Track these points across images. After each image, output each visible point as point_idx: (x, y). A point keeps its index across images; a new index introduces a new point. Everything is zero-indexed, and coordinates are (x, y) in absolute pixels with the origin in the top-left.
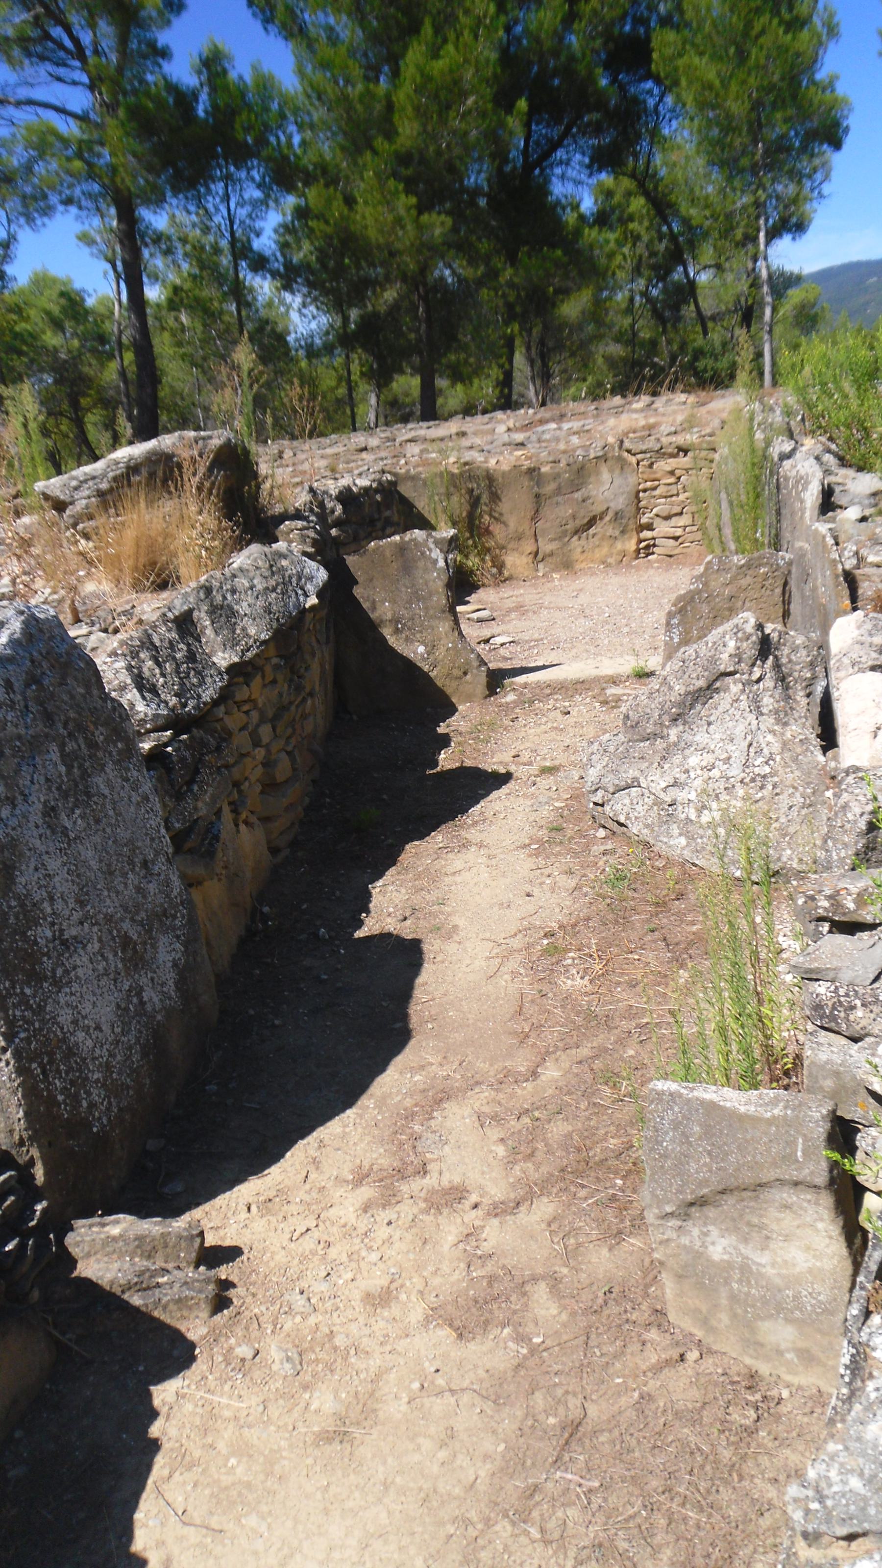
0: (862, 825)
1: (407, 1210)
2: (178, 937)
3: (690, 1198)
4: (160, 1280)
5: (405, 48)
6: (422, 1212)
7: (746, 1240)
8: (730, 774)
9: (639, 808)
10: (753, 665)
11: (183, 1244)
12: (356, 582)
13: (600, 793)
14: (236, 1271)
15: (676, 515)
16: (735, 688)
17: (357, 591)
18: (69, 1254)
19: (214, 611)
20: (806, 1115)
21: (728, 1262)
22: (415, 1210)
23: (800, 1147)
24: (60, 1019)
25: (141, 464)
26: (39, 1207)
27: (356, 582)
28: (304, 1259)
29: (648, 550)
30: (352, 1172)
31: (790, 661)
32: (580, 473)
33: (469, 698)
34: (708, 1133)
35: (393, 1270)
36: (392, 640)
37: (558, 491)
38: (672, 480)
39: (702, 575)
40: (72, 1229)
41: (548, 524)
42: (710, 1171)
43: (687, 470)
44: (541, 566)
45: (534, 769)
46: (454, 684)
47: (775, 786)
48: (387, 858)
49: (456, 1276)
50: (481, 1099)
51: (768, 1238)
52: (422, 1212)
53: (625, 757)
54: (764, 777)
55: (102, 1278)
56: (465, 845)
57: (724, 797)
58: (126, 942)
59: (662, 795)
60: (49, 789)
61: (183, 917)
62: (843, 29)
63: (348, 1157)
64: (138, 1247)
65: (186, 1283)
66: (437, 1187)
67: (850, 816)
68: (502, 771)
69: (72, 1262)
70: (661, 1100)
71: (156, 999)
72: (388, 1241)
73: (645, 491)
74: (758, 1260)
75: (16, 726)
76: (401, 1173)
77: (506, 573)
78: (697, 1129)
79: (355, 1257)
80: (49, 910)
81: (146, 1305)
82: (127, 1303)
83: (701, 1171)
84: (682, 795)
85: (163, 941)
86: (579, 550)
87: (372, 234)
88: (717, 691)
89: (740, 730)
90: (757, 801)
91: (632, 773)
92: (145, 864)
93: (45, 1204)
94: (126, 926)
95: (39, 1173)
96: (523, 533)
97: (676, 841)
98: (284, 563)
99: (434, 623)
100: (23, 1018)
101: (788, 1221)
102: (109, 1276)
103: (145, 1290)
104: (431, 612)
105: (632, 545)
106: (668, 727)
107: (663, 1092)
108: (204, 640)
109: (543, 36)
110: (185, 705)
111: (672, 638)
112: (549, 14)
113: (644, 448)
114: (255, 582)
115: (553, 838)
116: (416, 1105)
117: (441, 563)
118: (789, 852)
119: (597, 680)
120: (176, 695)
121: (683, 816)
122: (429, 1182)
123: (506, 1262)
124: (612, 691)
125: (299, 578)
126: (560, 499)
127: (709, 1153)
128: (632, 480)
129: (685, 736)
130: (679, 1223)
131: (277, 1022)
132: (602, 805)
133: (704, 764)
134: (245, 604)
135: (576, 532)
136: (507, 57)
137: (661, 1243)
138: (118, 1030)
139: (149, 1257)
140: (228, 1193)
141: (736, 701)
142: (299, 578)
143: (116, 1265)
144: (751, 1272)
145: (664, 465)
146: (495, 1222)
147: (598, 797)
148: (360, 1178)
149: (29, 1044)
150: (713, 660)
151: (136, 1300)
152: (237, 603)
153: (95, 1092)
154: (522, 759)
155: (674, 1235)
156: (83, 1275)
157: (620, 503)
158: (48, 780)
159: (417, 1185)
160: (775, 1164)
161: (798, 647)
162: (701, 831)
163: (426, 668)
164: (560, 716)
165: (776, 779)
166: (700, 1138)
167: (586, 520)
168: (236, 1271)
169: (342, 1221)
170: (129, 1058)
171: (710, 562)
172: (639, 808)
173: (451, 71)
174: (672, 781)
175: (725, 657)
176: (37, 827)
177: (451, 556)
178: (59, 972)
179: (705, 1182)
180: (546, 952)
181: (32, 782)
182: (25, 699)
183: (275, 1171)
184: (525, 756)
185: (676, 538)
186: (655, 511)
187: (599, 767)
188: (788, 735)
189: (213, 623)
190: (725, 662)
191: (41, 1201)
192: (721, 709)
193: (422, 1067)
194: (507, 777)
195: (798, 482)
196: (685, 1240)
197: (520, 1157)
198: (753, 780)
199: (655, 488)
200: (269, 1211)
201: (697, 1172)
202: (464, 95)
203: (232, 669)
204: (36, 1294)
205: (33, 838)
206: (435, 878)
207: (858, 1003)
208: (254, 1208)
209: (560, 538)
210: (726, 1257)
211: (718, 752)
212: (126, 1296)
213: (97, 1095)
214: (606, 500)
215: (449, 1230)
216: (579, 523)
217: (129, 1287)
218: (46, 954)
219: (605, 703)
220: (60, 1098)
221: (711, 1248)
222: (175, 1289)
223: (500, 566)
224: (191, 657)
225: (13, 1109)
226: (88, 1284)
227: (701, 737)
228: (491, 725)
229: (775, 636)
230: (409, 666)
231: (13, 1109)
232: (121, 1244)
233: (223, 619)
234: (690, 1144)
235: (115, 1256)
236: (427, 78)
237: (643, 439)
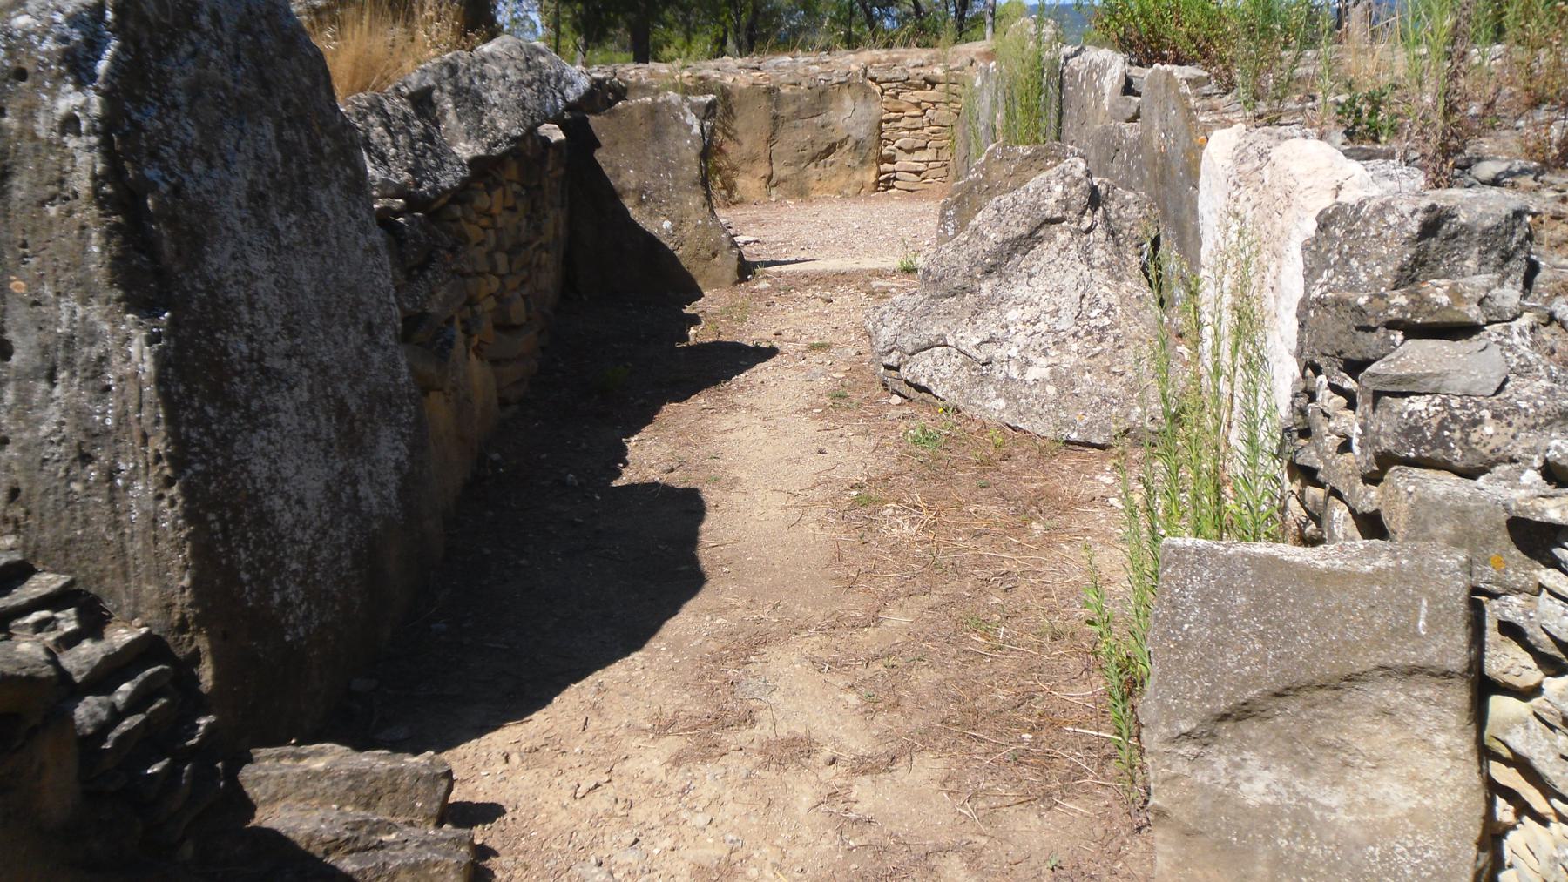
0: (1414, 227)
1: (738, 765)
2: (403, 435)
3: (1223, 706)
4: (385, 838)
6: (758, 767)
7: (1307, 771)
8: (1059, 328)
9: (944, 369)
10: (1083, 213)
11: (421, 788)
12: (599, 145)
13: (895, 355)
14: (497, 835)
15: (919, 148)
16: (1062, 237)
17: (600, 155)
18: (244, 795)
19: (458, 93)
20: (1433, 565)
21: (1274, 807)
22: (750, 765)
23: (1424, 612)
24: (251, 467)
26: (203, 721)
27: (599, 145)
28: (596, 820)
30: (649, 719)
31: (1119, 217)
32: (822, 97)
33: (716, 283)
34: (1261, 604)
35: (731, 837)
36: (634, 213)
37: (797, 115)
38: (918, 112)
39: (983, 165)
40: (250, 760)
42: (1264, 662)
43: (933, 103)
44: (774, 191)
45: (801, 345)
46: (701, 266)
47: (1117, 339)
48: (642, 417)
49: (824, 845)
50: (812, 642)
51: (1346, 764)
52: (758, 767)
53: (927, 312)
54: (1103, 329)
55: (294, 830)
56: (733, 408)
57: (1053, 353)
58: (342, 411)
59: (975, 353)
60: (259, 168)
61: (410, 411)
63: (641, 704)
64: (351, 788)
65: (424, 843)
66: (772, 738)
67: (1392, 219)
68: (765, 345)
69: (250, 808)
70: (1182, 561)
71: (374, 501)
72: (717, 800)
73: (888, 121)
74: (1325, 801)
75: (222, 70)
76: (721, 721)
77: (737, 196)
78: (1242, 600)
79: (672, 819)
80: (246, 318)
81: (363, 872)
82: (334, 868)
83: (1247, 664)
84: (999, 352)
85: (386, 433)
86: (816, 177)
88: (1040, 240)
89: (1070, 280)
90: (1095, 356)
91: (935, 330)
92: (369, 326)
93: (211, 718)
94: (343, 388)
95: (206, 675)
97: (993, 404)
98: (542, 60)
99: (683, 195)
100: (201, 444)
101: (1385, 735)
102: (306, 828)
103: (360, 850)
104: (681, 183)
105: (871, 177)
106: (979, 280)
107: (1186, 550)
108: (443, 126)
110: (419, 185)
111: (946, 231)
113: (890, 76)
114: (509, 72)
115: (837, 402)
116: (725, 648)
117: (696, 130)
118: (1138, 409)
119: (860, 272)
120: (409, 171)
121: (1001, 376)
122: (763, 731)
123: (894, 829)
125: (559, 80)
126: (798, 122)
127: (1262, 636)
128: (876, 109)
129: (1001, 290)
130: (1196, 750)
131: (522, 562)
132: (897, 369)
133: (1027, 317)
134: (495, 93)
135: (813, 159)
137: (1165, 781)
138: (327, 517)
139: (367, 806)
140: (474, 741)
142: (559, 80)
143: (317, 815)
144: (1312, 821)
146: (867, 780)
147: (892, 359)
148: (662, 728)
149: (208, 483)
150: (1036, 206)
151: (348, 865)
152: (486, 90)
153: (292, 588)
154: (784, 337)
155: (1187, 770)
156: (266, 825)
157: (861, 132)
158: (257, 157)
159: (742, 735)
160: (1378, 643)
161: (1128, 202)
163: (671, 246)
164: (821, 304)
165: (1118, 331)
166: (1246, 614)
168: (497, 835)
169: (646, 776)
170: (337, 560)
171: (992, 151)
172: (944, 369)
174: (987, 338)
175: (1051, 202)
176: (239, 206)
177: (707, 123)
178: (255, 405)
179: (1245, 683)
180: (856, 502)
181: (237, 149)
182: (237, 47)
183: (539, 718)
184: (789, 335)
185: (918, 173)
187: (894, 326)
188: (1124, 290)
189: (456, 106)
190: (1051, 207)
191: (206, 714)
192: (1044, 259)
193: (724, 611)
194: (772, 352)
195: (1090, 72)
196: (1202, 777)
197: (880, 705)
198: (1089, 333)
199: (899, 120)
200: (537, 763)
201: (1240, 666)
203: (475, 162)
204: (188, 850)
205: (232, 210)
206: (703, 436)
207: (1487, 414)
208: (515, 758)
209: (795, 164)
210: (1269, 799)
211: (1043, 304)
212: (330, 860)
213: (293, 592)
215: (803, 790)
216: (816, 149)
217: (336, 845)
218: (240, 374)
219: (871, 293)
220: (245, 577)
221: (1245, 787)
222: (409, 851)
223: (730, 188)
224: (428, 137)
225: (174, 573)
226: (275, 840)
227: (1021, 291)
228: (744, 308)
229: (1102, 189)
230: (652, 244)
231: (174, 573)
232: (326, 783)
233: (469, 105)
234: (1229, 624)
235: (315, 802)
237: (889, 68)
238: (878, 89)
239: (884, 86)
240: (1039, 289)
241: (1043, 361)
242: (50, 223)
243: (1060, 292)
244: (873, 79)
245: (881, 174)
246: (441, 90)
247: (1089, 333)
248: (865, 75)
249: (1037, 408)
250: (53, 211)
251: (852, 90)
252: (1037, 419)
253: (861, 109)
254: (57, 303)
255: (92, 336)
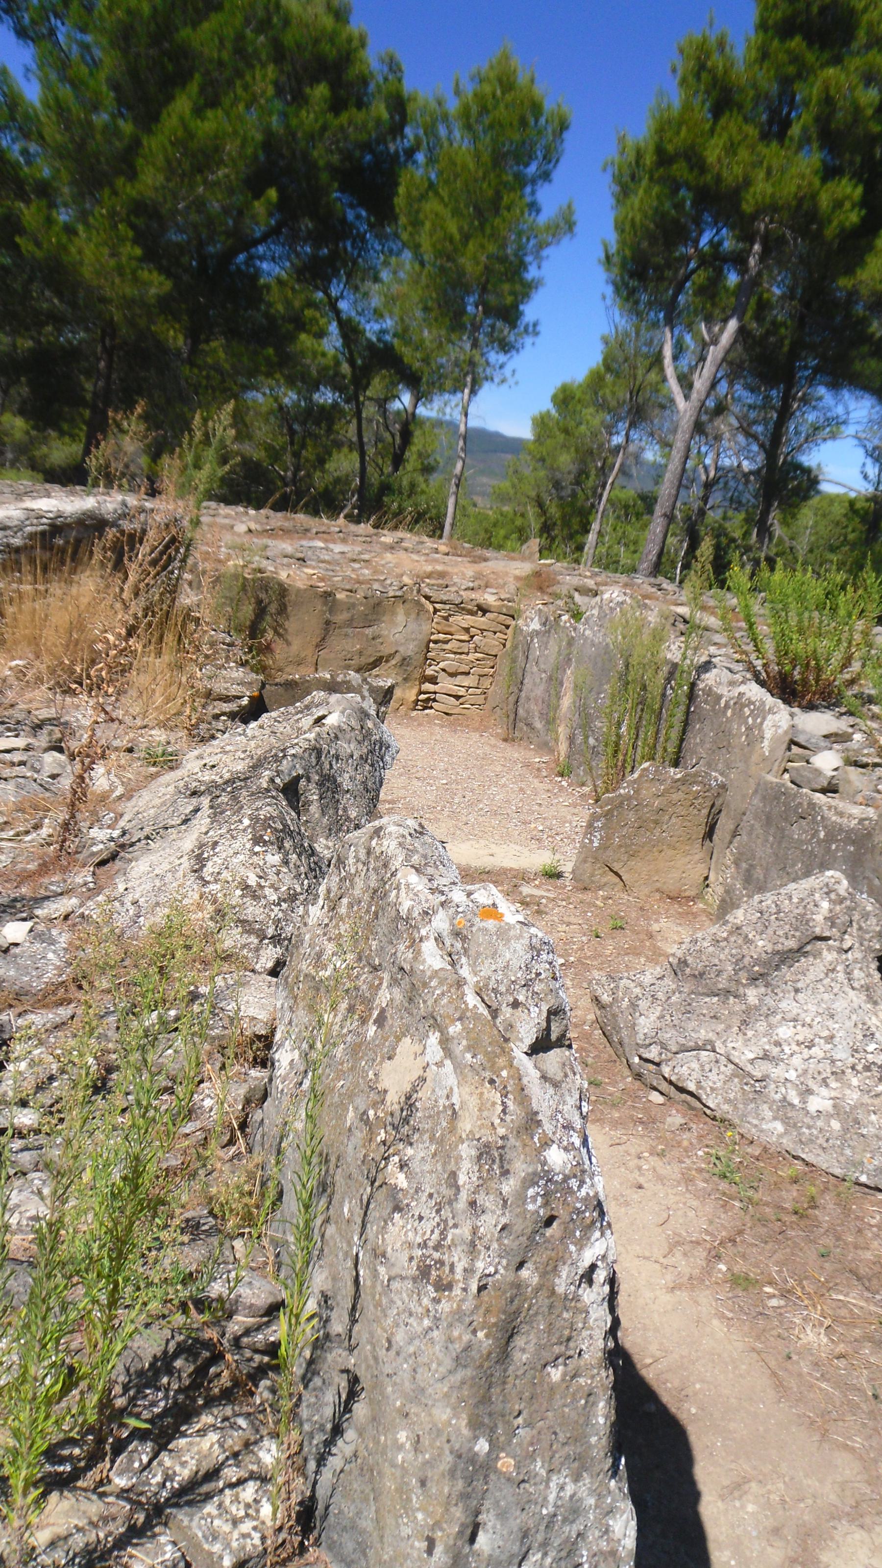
5: (170, 98)
16: (829, 957)
25: (69, 526)
29: (427, 704)
32: (376, 608)
37: (350, 623)
38: (466, 637)
39: (635, 781)
41: (332, 655)
59: (749, 1068)
62: (577, 229)
73: (436, 642)
84: (777, 1072)
87: (87, 272)
88: (806, 954)
91: (703, 1034)
96: (304, 659)
105: (411, 695)
106: (744, 986)
109: (300, 135)
111: (591, 841)
112: (312, 116)
113: (445, 598)
121: (778, 1097)
124: (526, 890)
126: (350, 630)
128: (426, 627)
133: (800, 1038)
136: (269, 143)
141: (833, 970)
145: (462, 620)
147: (653, 1053)
157: (410, 649)
162: (807, 1120)
167: (372, 660)
172: (713, 1076)
173: (216, 137)
174: (761, 1054)
175: (819, 918)
185: (458, 697)
186: (442, 665)
187: (653, 1018)
198: (867, 1068)
199: (446, 642)
202: (221, 163)
211: (817, 1028)
214: (397, 643)
216: (364, 660)
236: (191, 135)
238: (431, 610)
239: (437, 606)
240: (807, 1006)
241: (824, 1092)
242: (552, 1389)
243: (832, 1016)
244: (427, 598)
245: (421, 693)
246: (309, 780)
247: (867, 1068)
248: (419, 591)
249: (821, 1141)
250: (556, 1374)
251: (407, 605)
252: (820, 1151)
253: (412, 626)
254: (548, 1480)
255: (574, 1510)
